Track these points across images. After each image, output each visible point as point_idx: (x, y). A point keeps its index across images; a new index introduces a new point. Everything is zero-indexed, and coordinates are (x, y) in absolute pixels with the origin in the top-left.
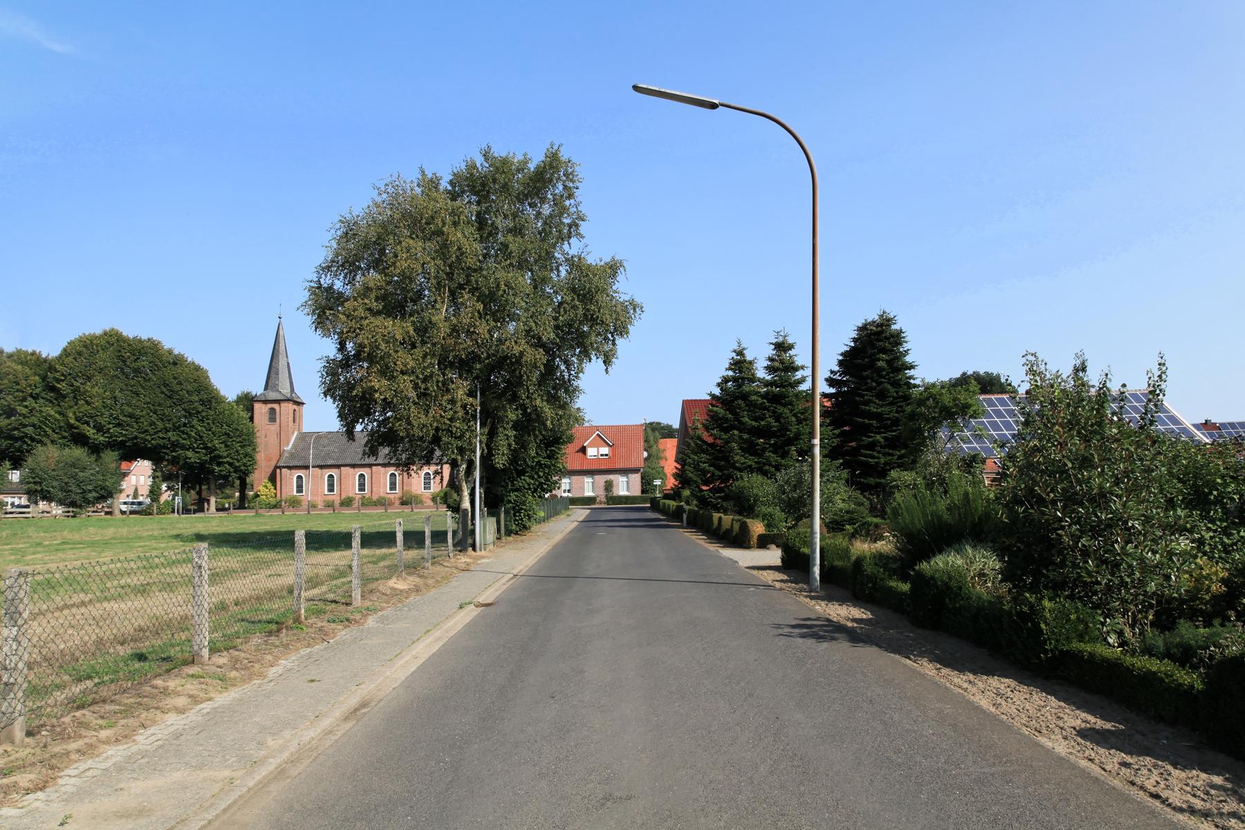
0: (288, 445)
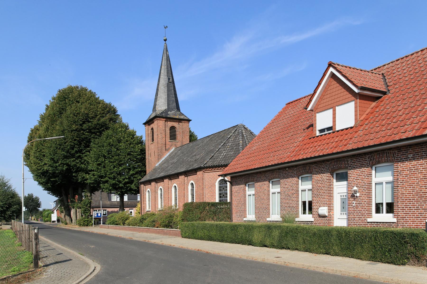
0: (159, 159)
